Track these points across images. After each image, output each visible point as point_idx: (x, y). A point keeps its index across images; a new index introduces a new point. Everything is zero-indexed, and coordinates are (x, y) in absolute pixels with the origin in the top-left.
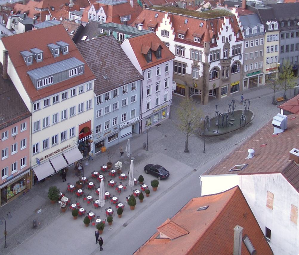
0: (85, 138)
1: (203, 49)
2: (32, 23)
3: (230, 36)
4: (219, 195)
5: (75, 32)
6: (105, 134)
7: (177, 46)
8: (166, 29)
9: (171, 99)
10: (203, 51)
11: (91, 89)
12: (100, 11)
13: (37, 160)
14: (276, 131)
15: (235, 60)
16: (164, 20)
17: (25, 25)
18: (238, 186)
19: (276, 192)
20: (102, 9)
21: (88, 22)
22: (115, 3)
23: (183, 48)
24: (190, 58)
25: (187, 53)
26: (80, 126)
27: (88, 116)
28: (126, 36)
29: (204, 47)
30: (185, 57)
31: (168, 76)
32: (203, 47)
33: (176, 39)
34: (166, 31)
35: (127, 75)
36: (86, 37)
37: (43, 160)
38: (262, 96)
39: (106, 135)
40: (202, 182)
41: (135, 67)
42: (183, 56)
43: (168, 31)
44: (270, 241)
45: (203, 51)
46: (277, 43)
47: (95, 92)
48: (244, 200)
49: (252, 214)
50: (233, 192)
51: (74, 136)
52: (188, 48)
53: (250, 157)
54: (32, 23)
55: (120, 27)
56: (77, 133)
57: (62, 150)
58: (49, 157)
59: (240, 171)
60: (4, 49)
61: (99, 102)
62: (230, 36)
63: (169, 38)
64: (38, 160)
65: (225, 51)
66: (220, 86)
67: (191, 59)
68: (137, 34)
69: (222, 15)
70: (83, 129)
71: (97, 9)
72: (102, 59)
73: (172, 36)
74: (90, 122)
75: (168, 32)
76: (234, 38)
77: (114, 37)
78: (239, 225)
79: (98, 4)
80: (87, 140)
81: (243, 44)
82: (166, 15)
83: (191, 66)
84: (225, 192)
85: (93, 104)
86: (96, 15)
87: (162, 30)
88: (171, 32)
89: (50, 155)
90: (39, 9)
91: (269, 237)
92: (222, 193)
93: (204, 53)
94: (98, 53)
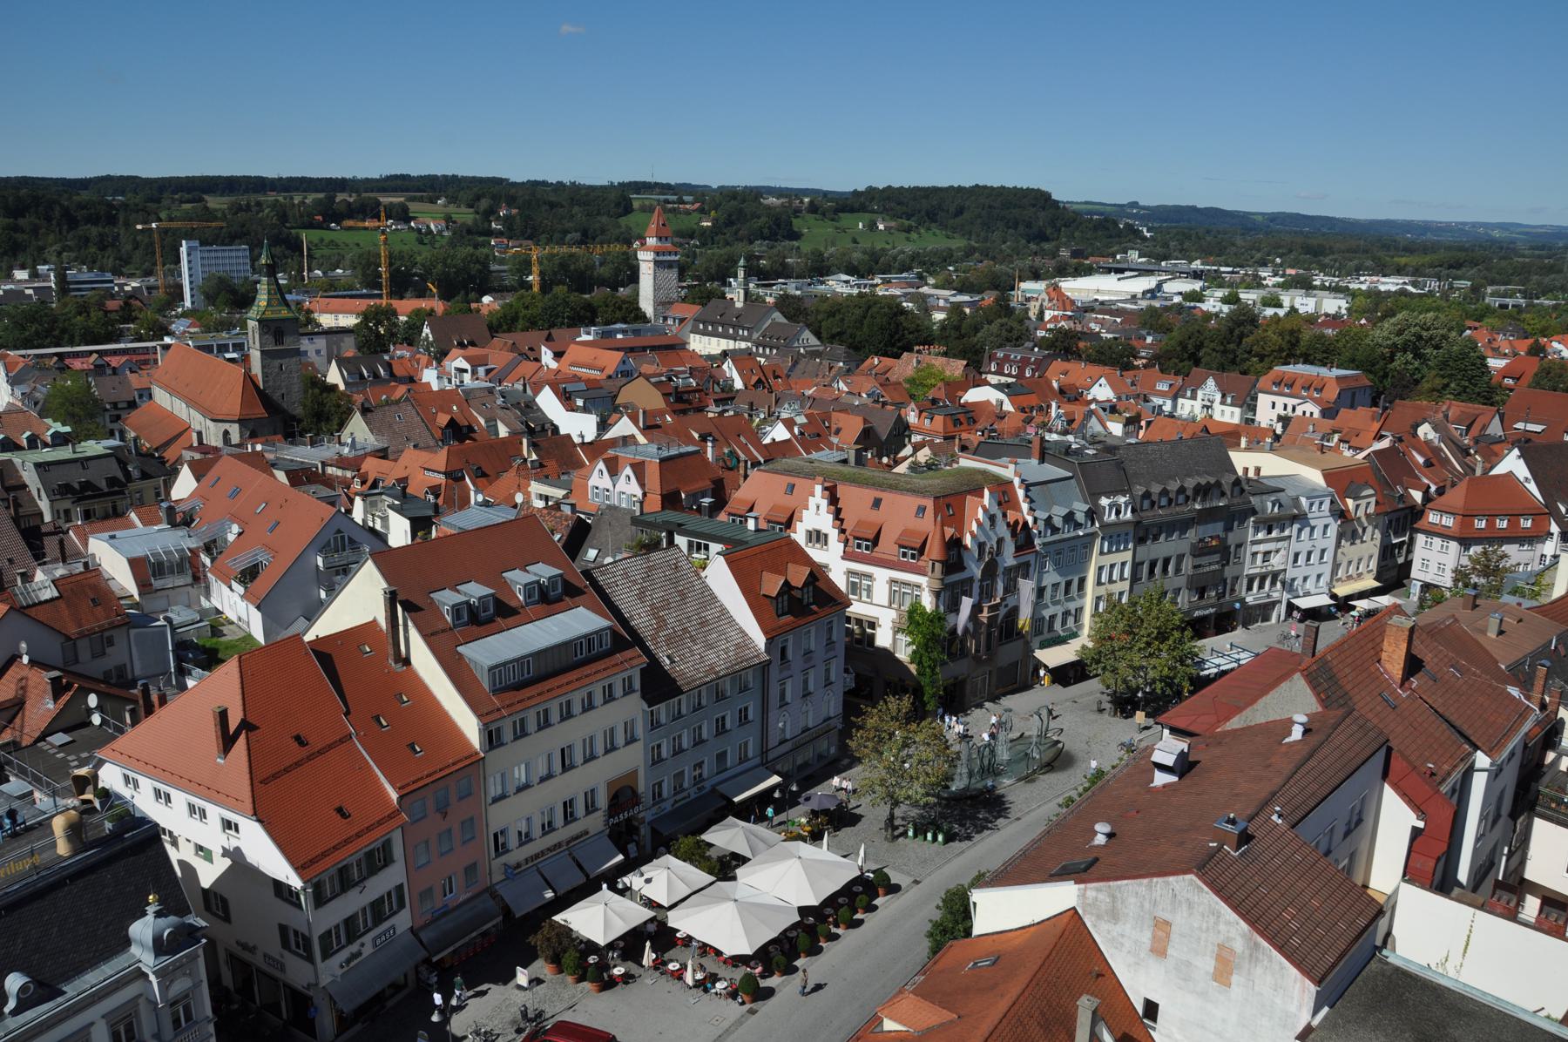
0: (626, 814)
1: (927, 579)
2: (430, 513)
3: (1000, 541)
4: (1024, 931)
5: (565, 538)
6: (676, 802)
7: (850, 573)
8: (818, 528)
9: (841, 711)
10: (925, 585)
11: (634, 691)
12: (623, 478)
13: (506, 870)
14: (1161, 779)
15: (1010, 606)
16: (812, 502)
17: (409, 519)
18: (1074, 908)
19: (1179, 920)
20: (628, 471)
21: (599, 509)
22: (665, 454)
23: (869, 577)
24: (887, 605)
25: (881, 592)
26: (610, 784)
27: (631, 759)
28: (106, 490)
29: (930, 574)
30: (874, 602)
31: (831, 654)
32: (924, 575)
33: (847, 556)
34: (818, 532)
35: (726, 653)
36: (596, 551)
37: (519, 870)
38: (1081, 696)
39: (677, 805)
40: (975, 904)
41: (743, 632)
42: (869, 600)
43: (824, 531)
44: (1154, 1029)
45: (925, 585)
46: (1127, 556)
47: (643, 697)
48: (1091, 941)
49: (1110, 971)
50: (1065, 919)
51: (597, 810)
52: (882, 576)
53: (1100, 840)
54: (430, 513)
55: (691, 520)
56: (602, 801)
57: (568, 842)
58: (535, 862)
59: (1082, 870)
60: (385, 585)
61: (654, 724)
62: (1000, 541)
63: (827, 550)
64: (509, 867)
65: (985, 583)
66: (969, 676)
67: (890, 607)
68: (747, 542)
69: (974, 485)
70: (617, 792)
71: (613, 471)
72: (654, 611)
73: (836, 547)
74: (634, 774)
75: (826, 536)
76: (1009, 548)
77: (679, 548)
78: (1087, 993)
79: (616, 458)
80: (629, 820)
81: (1032, 562)
82: (818, 489)
83: (891, 625)
84: (1038, 923)
85: (639, 731)
86: (611, 488)
87: (808, 531)
88: (833, 534)
89: (537, 856)
90: (439, 472)
91: (1154, 1020)
92: (1029, 926)
93: (927, 589)
94: (641, 596)
